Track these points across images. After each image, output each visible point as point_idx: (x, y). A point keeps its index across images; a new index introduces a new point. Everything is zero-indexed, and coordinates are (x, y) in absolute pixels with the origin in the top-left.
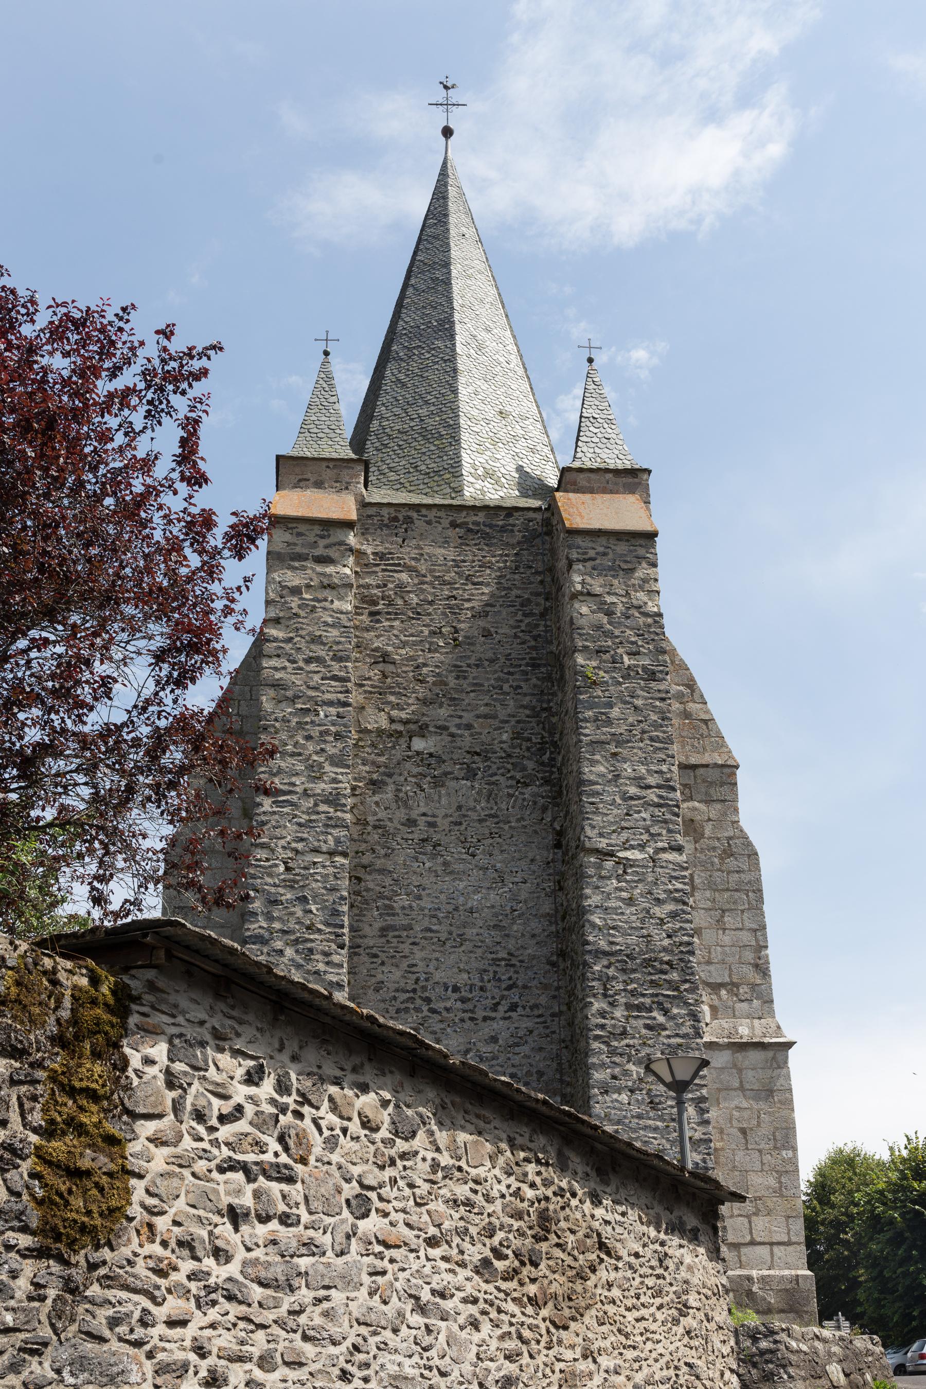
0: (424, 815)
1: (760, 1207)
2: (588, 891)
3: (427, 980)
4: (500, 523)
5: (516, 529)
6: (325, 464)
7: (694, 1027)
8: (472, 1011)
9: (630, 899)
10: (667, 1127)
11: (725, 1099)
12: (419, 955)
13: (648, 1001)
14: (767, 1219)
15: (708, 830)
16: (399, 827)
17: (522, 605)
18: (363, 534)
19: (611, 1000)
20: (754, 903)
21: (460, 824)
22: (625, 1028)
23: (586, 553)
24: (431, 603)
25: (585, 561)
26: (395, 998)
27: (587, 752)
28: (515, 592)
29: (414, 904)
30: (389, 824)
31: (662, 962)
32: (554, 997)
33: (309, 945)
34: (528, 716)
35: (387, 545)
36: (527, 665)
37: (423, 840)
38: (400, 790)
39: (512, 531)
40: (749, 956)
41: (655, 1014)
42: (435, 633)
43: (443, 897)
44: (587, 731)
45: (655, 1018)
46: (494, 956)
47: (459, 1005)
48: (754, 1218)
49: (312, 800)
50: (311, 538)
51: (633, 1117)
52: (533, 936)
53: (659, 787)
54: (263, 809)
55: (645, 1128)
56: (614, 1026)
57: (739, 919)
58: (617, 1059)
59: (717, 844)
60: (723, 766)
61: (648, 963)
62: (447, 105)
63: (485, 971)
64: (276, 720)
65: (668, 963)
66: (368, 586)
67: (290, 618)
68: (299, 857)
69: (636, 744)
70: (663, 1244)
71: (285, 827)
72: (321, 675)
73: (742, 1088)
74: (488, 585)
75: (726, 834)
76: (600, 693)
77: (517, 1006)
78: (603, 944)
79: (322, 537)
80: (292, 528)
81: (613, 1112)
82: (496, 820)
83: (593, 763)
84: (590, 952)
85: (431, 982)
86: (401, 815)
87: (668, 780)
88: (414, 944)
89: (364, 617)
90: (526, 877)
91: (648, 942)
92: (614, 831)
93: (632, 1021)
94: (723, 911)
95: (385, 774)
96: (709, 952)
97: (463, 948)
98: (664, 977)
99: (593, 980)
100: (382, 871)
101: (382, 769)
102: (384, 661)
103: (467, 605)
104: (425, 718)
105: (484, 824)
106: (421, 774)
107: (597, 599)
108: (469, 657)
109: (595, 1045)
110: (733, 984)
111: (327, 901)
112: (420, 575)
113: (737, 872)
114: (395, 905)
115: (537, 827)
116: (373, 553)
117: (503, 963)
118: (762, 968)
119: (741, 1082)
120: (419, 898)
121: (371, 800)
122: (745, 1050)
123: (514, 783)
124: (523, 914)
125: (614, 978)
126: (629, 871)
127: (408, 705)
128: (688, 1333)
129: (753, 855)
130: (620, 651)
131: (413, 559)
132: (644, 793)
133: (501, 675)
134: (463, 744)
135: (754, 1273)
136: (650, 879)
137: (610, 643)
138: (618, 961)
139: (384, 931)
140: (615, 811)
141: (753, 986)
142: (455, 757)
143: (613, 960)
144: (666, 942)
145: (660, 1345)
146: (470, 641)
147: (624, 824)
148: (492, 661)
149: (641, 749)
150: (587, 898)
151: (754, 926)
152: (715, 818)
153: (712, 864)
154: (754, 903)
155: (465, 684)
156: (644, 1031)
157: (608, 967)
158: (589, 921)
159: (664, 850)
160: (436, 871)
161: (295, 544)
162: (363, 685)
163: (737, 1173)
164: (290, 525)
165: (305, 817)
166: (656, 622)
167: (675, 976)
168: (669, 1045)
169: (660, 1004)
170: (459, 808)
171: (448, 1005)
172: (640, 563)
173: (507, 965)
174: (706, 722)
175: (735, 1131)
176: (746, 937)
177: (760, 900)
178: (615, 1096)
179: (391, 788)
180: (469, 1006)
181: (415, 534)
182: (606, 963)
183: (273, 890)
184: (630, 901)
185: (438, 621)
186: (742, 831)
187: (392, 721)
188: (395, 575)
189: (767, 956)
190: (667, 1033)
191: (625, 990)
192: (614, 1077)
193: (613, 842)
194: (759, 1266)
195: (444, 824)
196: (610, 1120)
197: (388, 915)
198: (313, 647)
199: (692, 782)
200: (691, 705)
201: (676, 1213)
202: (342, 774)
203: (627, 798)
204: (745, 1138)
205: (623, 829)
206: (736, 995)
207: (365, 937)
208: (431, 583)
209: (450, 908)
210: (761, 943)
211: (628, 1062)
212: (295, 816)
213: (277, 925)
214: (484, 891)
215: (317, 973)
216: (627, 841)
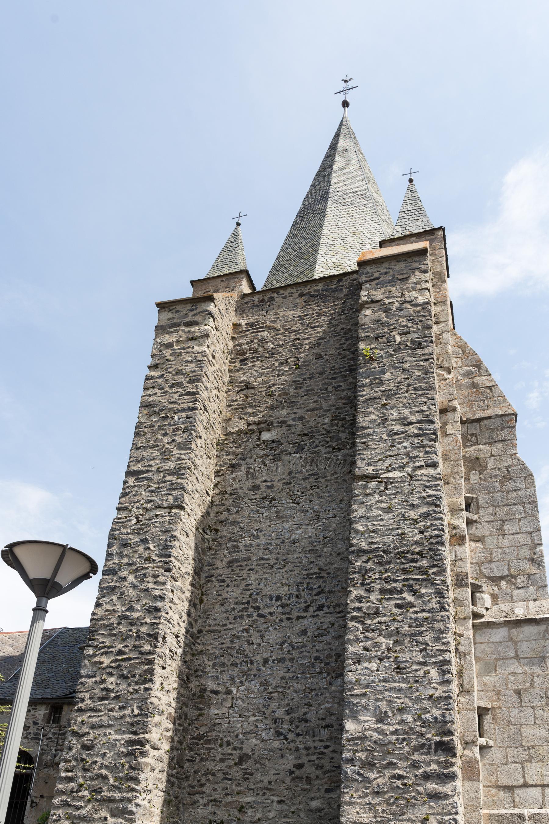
0: (265, 481)
2: (355, 507)
3: (258, 594)
4: (333, 287)
6: (220, 279)
7: (439, 602)
8: (289, 613)
9: (389, 508)
10: (411, 687)
11: (502, 666)
12: (253, 576)
13: (399, 585)
15: (490, 464)
16: (248, 492)
17: (345, 334)
18: (241, 314)
19: (367, 587)
20: (530, 512)
21: (290, 483)
22: (378, 609)
23: (372, 276)
24: (281, 346)
25: (371, 281)
26: (234, 609)
27: (362, 407)
28: (341, 326)
29: (253, 542)
30: (240, 491)
31: (413, 553)
33: (144, 572)
34: (344, 404)
35: (255, 317)
36: (346, 371)
37: (263, 498)
38: (250, 468)
40: (525, 552)
41: (405, 595)
42: (282, 363)
43: (274, 535)
44: (364, 393)
45: (404, 599)
46: (308, 572)
48: (527, 764)
49: (162, 475)
50: (184, 312)
51: (380, 681)
52: (339, 554)
53: (419, 422)
54: (128, 485)
55: (391, 689)
56: (368, 608)
57: (517, 526)
58: (369, 635)
59: (498, 472)
60: (503, 415)
61: (401, 555)
62: (345, 91)
63: (301, 583)
64: (146, 427)
65: (419, 553)
66: (241, 345)
67: (164, 363)
68: (148, 513)
69: (402, 395)
71: (141, 494)
72: (179, 394)
73: (517, 657)
74: (322, 326)
75: (506, 464)
76: (376, 365)
78: (364, 545)
79: (192, 310)
80: (172, 310)
81: (362, 677)
82: (316, 477)
83: (366, 414)
84: (353, 552)
85: (261, 595)
86: (250, 483)
87: (427, 416)
88: (251, 570)
89: (237, 364)
90: (336, 513)
91: (402, 538)
92: (380, 460)
93: (385, 603)
94: (503, 521)
96: (491, 554)
97: (286, 569)
98: (414, 565)
99: (353, 573)
100: (233, 523)
101: (239, 456)
102: (248, 388)
103: (306, 342)
104: (271, 418)
105: (307, 481)
106: (265, 455)
107: (379, 304)
108: (305, 374)
109: (352, 624)
110: (511, 576)
111: (161, 540)
112: (275, 330)
113: (515, 491)
114: (240, 544)
115: (346, 477)
116: (246, 324)
117: (315, 576)
118: (537, 561)
120: (257, 537)
121: (229, 477)
122: (520, 626)
123: (331, 449)
124: (332, 539)
125: (371, 570)
127: (260, 412)
129: (529, 477)
130: (394, 333)
131: (272, 321)
132: (406, 428)
133: (327, 380)
134: (296, 430)
135: (526, 812)
136: (406, 491)
137: (386, 330)
138: (376, 556)
139: (230, 564)
140: (382, 445)
141: (529, 576)
142: (289, 440)
143: (371, 556)
144: (418, 537)
146: (306, 364)
147: (388, 453)
148: (321, 373)
149: (406, 397)
150: (353, 511)
151: (530, 529)
152: (497, 454)
153: (494, 488)
154: (530, 512)
155: (301, 392)
156: (394, 610)
157: (366, 562)
158: (353, 529)
159: (420, 467)
160: (270, 518)
163: (512, 727)
164: (171, 308)
165: (156, 486)
166: (423, 308)
167: (424, 563)
168: (416, 619)
169: (410, 586)
170: (290, 473)
171: (272, 610)
172: (414, 273)
173: (317, 577)
174: (490, 388)
175: (511, 693)
176: (523, 539)
177: (536, 509)
178: (366, 665)
179: (244, 467)
181: (275, 307)
182: (365, 558)
183: (125, 537)
184: (389, 510)
185: (285, 354)
186: (519, 460)
187: (249, 424)
188: (259, 334)
189: (541, 551)
190: (415, 609)
191: (380, 578)
192: (366, 649)
193: (378, 468)
194: (532, 804)
195: (278, 485)
196: (360, 685)
197: (235, 552)
198: (176, 377)
199: (478, 431)
200: (478, 378)
202: (185, 454)
203: (392, 434)
204: (520, 698)
205: (387, 457)
206: (514, 584)
207: (217, 569)
208: (283, 335)
209: (279, 542)
210: (536, 542)
211: (379, 636)
212: (149, 486)
213: (125, 561)
214: (304, 527)
215: (146, 590)
216: (390, 465)
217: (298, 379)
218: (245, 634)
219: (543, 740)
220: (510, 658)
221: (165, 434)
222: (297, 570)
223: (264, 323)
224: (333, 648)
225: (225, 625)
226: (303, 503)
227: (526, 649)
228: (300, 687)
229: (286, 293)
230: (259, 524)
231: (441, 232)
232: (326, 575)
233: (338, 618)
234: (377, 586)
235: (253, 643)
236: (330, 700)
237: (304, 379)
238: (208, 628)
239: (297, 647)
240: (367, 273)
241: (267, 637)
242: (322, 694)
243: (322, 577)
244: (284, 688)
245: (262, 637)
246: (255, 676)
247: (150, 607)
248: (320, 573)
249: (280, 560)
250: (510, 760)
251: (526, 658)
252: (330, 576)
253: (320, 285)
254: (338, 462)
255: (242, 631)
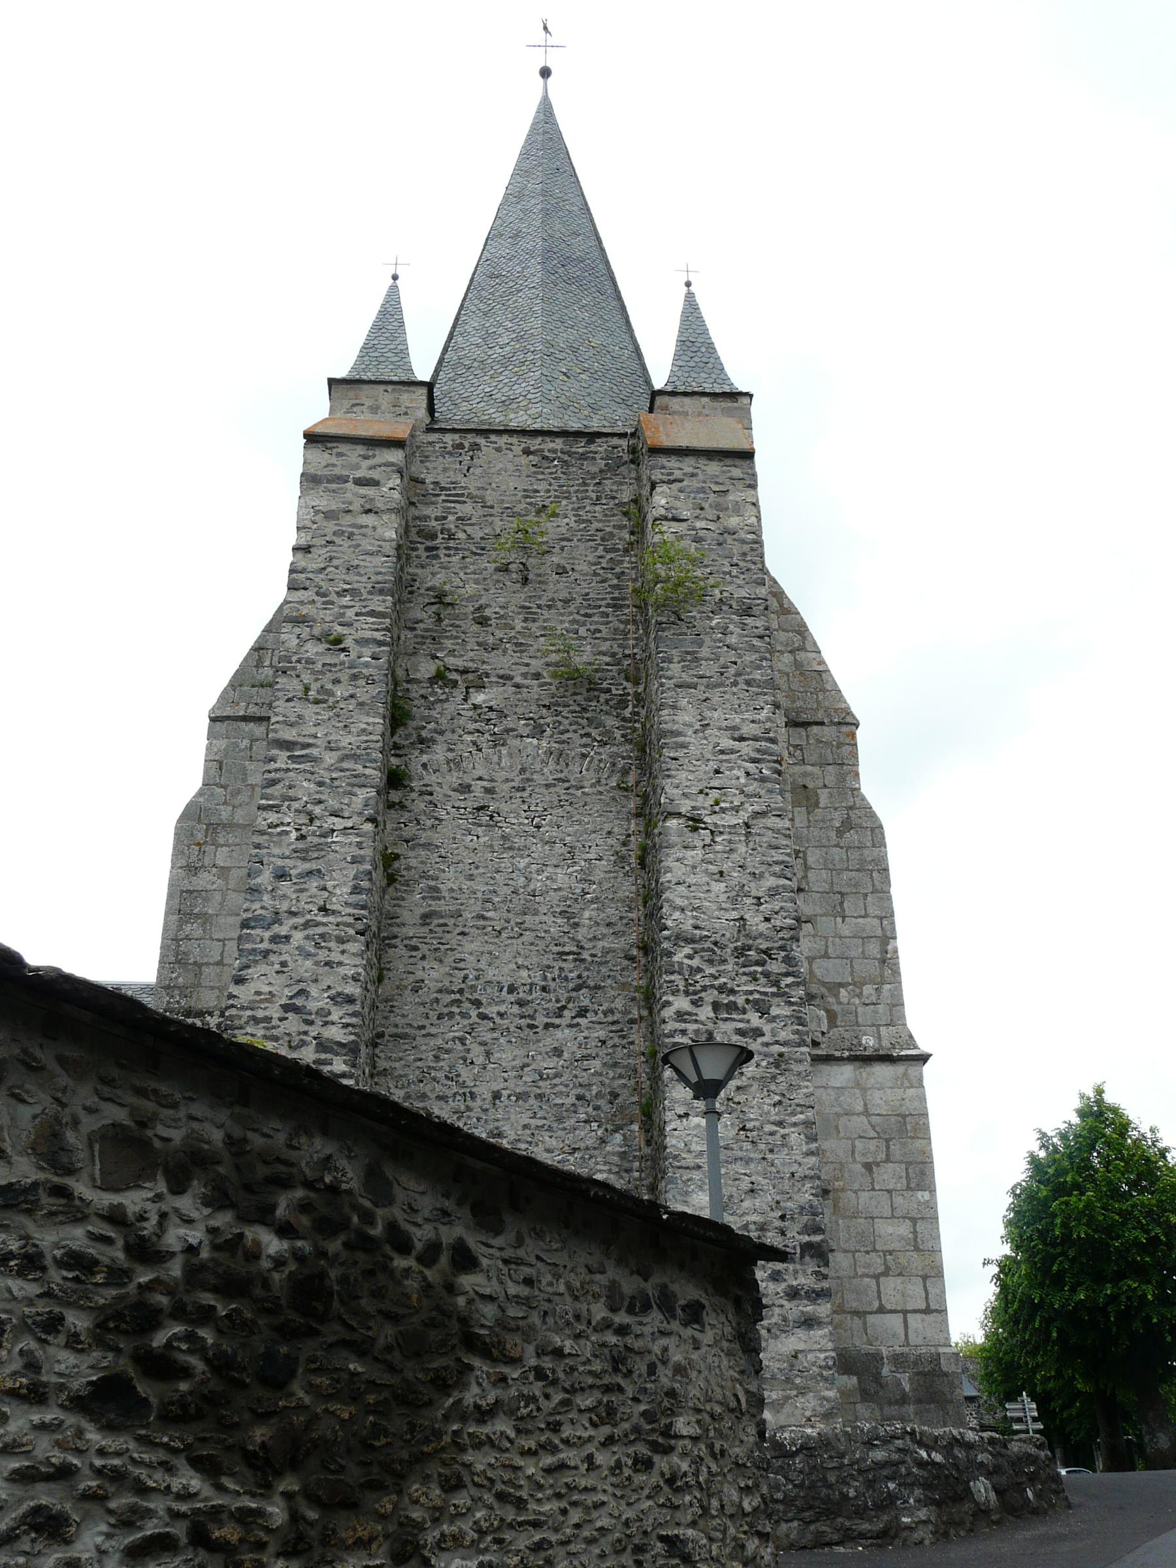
1: (891, 1264)
3: (477, 978)
5: (598, 456)
6: (382, 387)
8: (532, 1017)
14: (899, 1280)
17: (603, 539)
21: (524, 789)
26: (437, 1000)
28: (596, 525)
32: (633, 999)
33: (320, 930)
34: (607, 664)
36: (608, 605)
37: (479, 809)
39: (594, 458)
46: (560, 949)
47: (516, 1009)
54: (277, 765)
56: (697, 1032)
63: (549, 967)
64: (299, 661)
70: (622, 1331)
77: (587, 1011)
79: (366, 458)
80: (331, 448)
82: (567, 785)
84: (667, 938)
87: (768, 731)
88: (463, 934)
95: (435, 731)
102: (440, 603)
104: (485, 667)
105: (552, 790)
117: (571, 957)
119: (865, 1105)
126: (718, 839)
128: (671, 1481)
133: (578, 617)
138: (703, 950)
139: (426, 917)
145: (603, 1511)
148: (566, 602)
155: (534, 627)
161: (334, 465)
162: (415, 629)
164: (329, 445)
170: (523, 770)
171: (502, 1009)
173: (575, 960)
175: (858, 1168)
180: (528, 1010)
182: (687, 950)
188: (457, 506)
197: (433, 898)
201: (656, 1279)
214: (550, 869)
217: (527, 604)
218: (459, 1046)
219: (903, 1243)
220: (858, 1114)
221: (337, 681)
222: (541, 945)
223: (465, 488)
224: (607, 1081)
225: (423, 1027)
226: (547, 828)
227: (880, 1102)
228: (554, 1143)
229: (502, 440)
230: (472, 854)
231: (746, 400)
232: (589, 959)
233: (612, 1032)
234: (710, 996)
235: (472, 1063)
236: (603, 1168)
237: (539, 607)
238: (393, 1030)
239: (548, 1075)
240: (663, 467)
241: (497, 1055)
242: (591, 1157)
243: (583, 960)
244: (530, 1143)
245: (488, 1054)
246: (478, 1119)
247: (339, 994)
248: (579, 954)
249: (512, 923)
250: (860, 1271)
251: (879, 1115)
252: (596, 959)
253: (557, 440)
254: (602, 765)
255: (453, 1039)
